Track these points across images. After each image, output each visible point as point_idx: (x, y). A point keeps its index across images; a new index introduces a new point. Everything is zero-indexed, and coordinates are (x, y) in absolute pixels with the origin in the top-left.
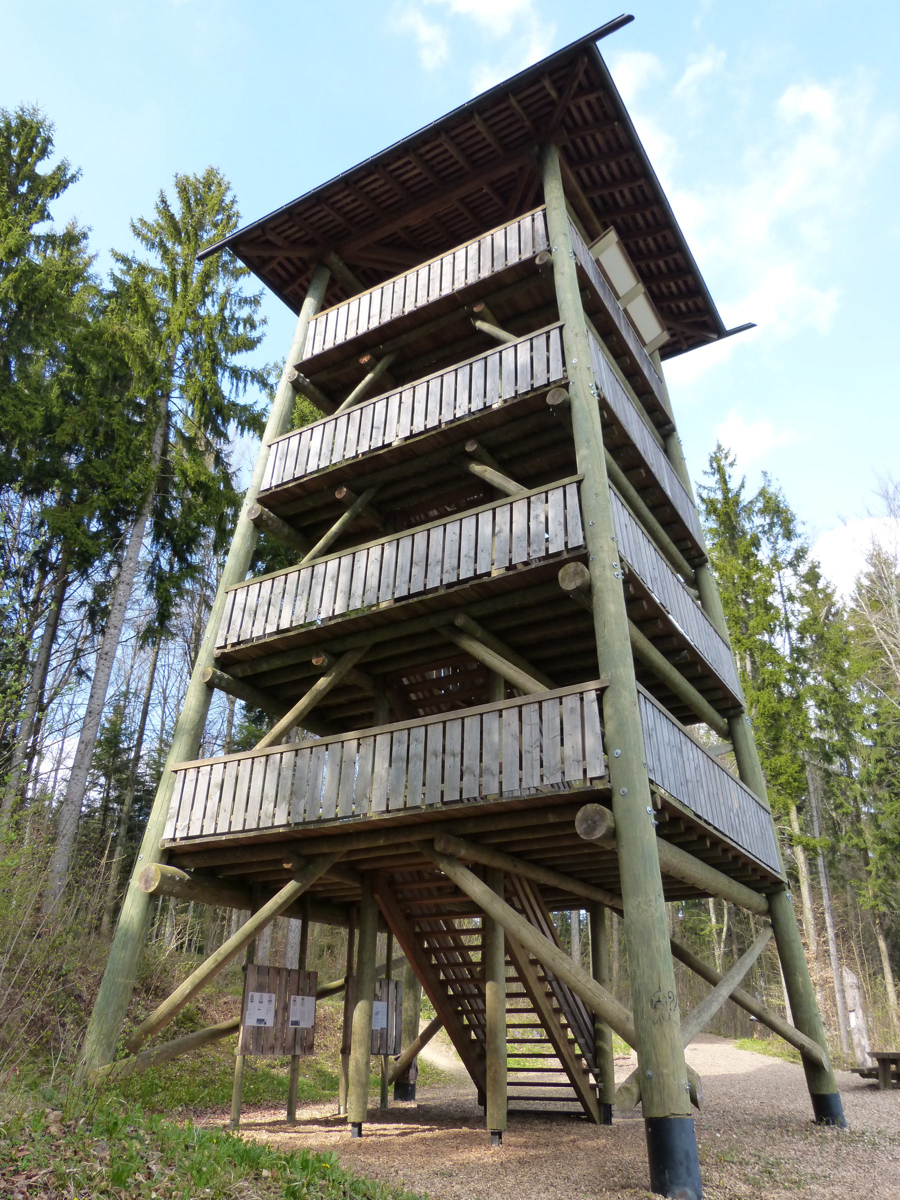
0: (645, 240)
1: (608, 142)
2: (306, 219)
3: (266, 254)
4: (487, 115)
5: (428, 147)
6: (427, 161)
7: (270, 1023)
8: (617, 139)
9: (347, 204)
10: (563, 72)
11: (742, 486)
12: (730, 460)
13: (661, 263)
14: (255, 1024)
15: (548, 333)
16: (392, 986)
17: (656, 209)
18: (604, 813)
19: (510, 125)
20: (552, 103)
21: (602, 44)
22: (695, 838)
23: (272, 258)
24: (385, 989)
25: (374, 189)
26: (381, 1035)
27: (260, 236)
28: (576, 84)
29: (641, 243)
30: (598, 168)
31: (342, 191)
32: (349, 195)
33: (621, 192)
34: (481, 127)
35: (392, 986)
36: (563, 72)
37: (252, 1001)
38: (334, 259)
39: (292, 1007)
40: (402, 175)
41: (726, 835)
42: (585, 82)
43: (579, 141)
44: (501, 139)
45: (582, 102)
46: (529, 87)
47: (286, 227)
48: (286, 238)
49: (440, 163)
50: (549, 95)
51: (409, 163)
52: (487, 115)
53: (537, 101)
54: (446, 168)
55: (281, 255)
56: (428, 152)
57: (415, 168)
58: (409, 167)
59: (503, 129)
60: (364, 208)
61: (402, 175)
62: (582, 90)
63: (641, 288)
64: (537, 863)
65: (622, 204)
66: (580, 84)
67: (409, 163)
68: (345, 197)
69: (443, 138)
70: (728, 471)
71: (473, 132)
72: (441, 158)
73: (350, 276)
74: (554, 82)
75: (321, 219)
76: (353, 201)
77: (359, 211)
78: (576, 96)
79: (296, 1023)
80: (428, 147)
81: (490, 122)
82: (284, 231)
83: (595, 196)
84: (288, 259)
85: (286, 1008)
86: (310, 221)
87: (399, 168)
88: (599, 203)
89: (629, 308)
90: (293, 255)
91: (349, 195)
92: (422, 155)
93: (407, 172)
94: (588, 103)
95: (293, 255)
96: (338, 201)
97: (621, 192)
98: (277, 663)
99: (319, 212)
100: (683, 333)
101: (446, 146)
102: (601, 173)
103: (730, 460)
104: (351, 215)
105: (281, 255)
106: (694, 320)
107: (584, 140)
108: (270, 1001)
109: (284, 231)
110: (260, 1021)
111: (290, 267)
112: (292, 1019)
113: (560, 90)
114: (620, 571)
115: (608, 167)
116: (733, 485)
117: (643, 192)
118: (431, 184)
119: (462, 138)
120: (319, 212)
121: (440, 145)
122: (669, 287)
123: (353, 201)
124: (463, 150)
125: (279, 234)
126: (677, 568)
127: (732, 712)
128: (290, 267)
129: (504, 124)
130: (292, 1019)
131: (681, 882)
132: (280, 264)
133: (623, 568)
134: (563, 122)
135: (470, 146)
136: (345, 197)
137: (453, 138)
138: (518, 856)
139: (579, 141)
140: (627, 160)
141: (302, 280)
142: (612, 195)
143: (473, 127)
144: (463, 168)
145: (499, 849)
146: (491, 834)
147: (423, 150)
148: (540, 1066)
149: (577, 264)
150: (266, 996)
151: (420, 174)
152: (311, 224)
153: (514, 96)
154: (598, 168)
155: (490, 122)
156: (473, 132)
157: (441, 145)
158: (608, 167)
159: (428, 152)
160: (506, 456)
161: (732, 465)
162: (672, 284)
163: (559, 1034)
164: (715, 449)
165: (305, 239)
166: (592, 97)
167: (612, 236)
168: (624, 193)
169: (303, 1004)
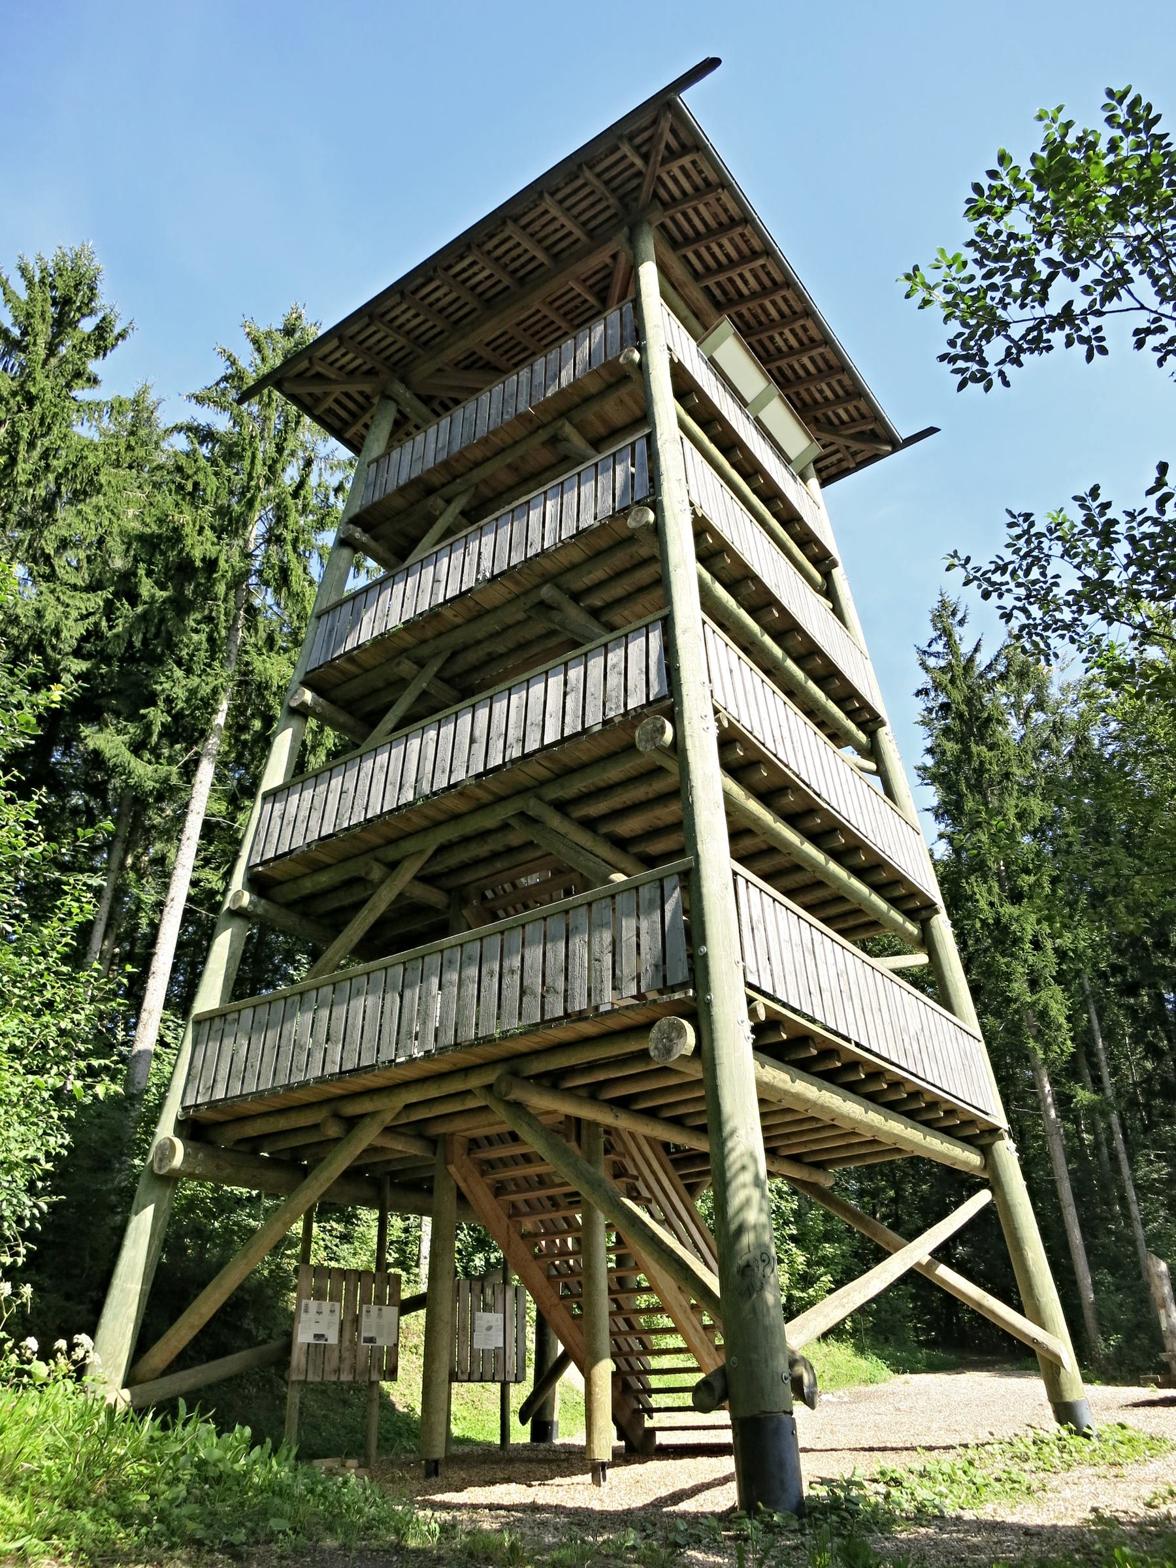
0: (781, 334)
1: (715, 216)
2: (361, 343)
3: (317, 390)
4: (560, 195)
5: (495, 241)
6: (498, 259)
7: (333, 1339)
8: (726, 210)
9: (408, 321)
10: (646, 135)
11: (976, 650)
12: (959, 616)
13: (806, 360)
14: (312, 1340)
15: (633, 444)
16: (510, 1294)
17: (789, 294)
18: (683, 1027)
19: (593, 205)
20: (639, 174)
21: (688, 98)
22: (814, 1052)
23: (326, 394)
24: (500, 1297)
25: (438, 300)
26: (496, 1357)
27: (307, 369)
28: (663, 146)
29: (777, 338)
30: (708, 249)
31: (399, 304)
32: (408, 309)
33: (741, 276)
34: (555, 211)
35: (510, 1294)
36: (646, 135)
37: (306, 1311)
38: (399, 389)
39: (364, 1321)
40: (469, 278)
41: (892, 1064)
42: (674, 144)
43: (679, 217)
44: (584, 224)
45: (675, 168)
46: (607, 156)
47: (337, 355)
48: (341, 368)
49: (514, 260)
50: (633, 165)
51: (474, 263)
52: (560, 195)
53: (621, 173)
54: (523, 266)
55: (337, 391)
56: (496, 247)
57: (483, 268)
58: (476, 269)
59: (584, 211)
60: (429, 324)
61: (469, 278)
62: (672, 155)
63: (775, 389)
64: (652, 1114)
65: (745, 291)
66: (668, 146)
67: (474, 263)
68: (404, 312)
69: (510, 229)
70: (958, 631)
71: (547, 218)
72: (514, 253)
73: (424, 410)
74: (637, 148)
75: (379, 341)
76: (416, 316)
77: (424, 328)
78: (664, 161)
79: (371, 1340)
80: (495, 241)
81: (567, 204)
82: (337, 360)
83: (711, 283)
84: (347, 395)
85: (356, 1320)
86: (367, 344)
87: (464, 270)
88: (717, 292)
89: (762, 416)
90: (353, 389)
91: (408, 309)
92: (489, 252)
93: (475, 274)
94: (683, 169)
95: (353, 389)
96: (397, 317)
97: (741, 276)
98: (324, 879)
99: (375, 333)
100: (848, 447)
101: (517, 239)
102: (713, 255)
103: (959, 616)
104: (417, 333)
105: (337, 391)
106: (858, 429)
107: (685, 214)
108: (332, 1311)
109: (337, 360)
110: (317, 1336)
111: (351, 405)
112: (364, 1334)
113: (645, 157)
114: (713, 726)
115: (721, 246)
116: (965, 648)
117: (768, 274)
118: (507, 288)
119: (536, 226)
120: (375, 333)
121: (509, 238)
122: (821, 392)
123: (416, 316)
124: (540, 241)
125: (331, 364)
126: (837, 737)
127: (924, 914)
128: (351, 405)
129: (584, 204)
130: (364, 1334)
131: (854, 1134)
132: (337, 401)
133: (718, 720)
134: (655, 195)
135: (546, 237)
136: (404, 312)
137: (524, 228)
138: (623, 1104)
139: (679, 217)
140: (742, 235)
141: (366, 418)
142: (730, 280)
143: (546, 212)
144: (542, 264)
145: (593, 1094)
146: (571, 1071)
147: (490, 245)
148: (666, 1377)
149: (672, 360)
150: (326, 1305)
151: (491, 276)
152: (369, 349)
153: (591, 168)
154: (708, 249)
155: (567, 204)
156: (547, 218)
157: (509, 238)
158: (721, 246)
159: (496, 247)
160: (598, 603)
161: (961, 622)
162: (824, 387)
163: (701, 1339)
164: (936, 605)
165: (365, 368)
166: (686, 161)
167: (726, 326)
168: (746, 278)
169: (380, 1316)
